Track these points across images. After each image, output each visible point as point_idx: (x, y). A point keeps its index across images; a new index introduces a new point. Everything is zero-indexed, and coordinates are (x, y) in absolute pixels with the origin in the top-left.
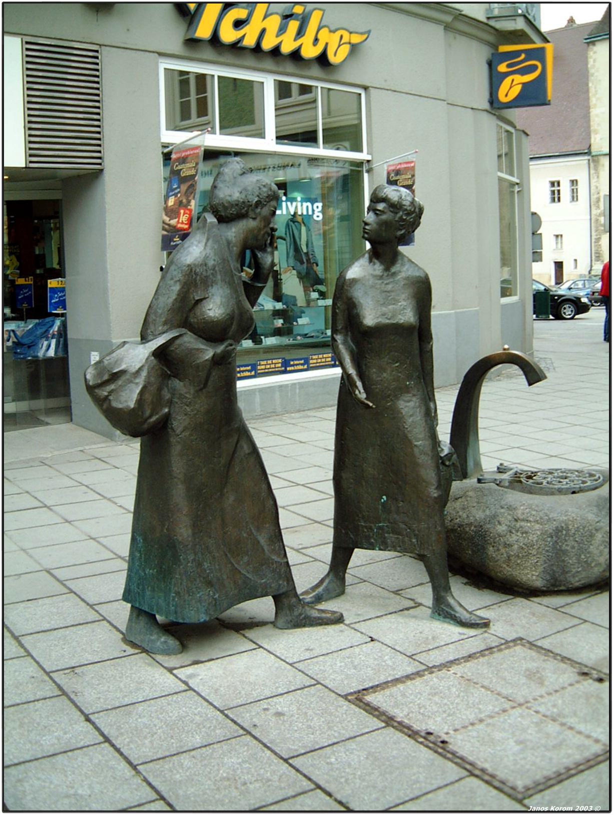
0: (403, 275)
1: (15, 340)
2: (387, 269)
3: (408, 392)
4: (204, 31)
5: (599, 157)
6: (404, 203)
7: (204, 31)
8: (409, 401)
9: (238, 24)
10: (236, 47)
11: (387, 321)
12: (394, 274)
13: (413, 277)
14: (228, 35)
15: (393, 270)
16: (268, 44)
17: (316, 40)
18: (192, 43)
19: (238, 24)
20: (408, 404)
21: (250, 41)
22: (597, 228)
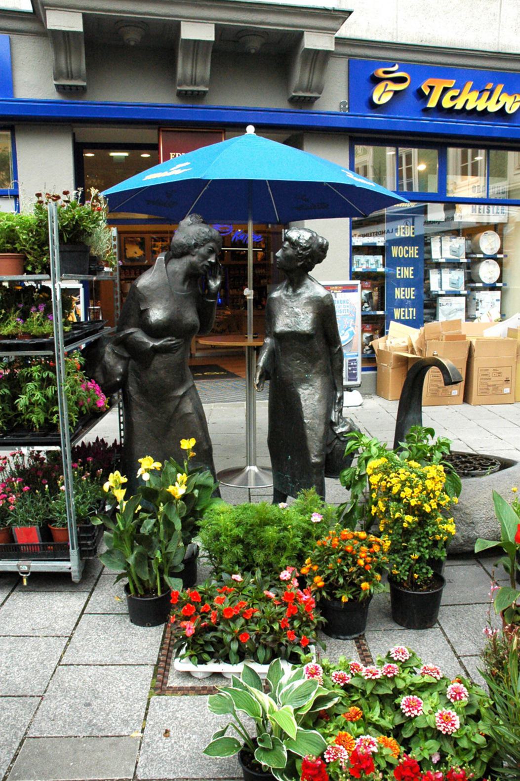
0: (306, 295)
1: (91, 302)
2: (294, 291)
3: (307, 383)
4: (432, 104)
5: (169, 272)
6: (301, 241)
7: (432, 104)
8: (305, 389)
9: (453, 98)
10: (451, 110)
11: (290, 330)
12: (300, 294)
13: (313, 297)
14: (447, 103)
15: (299, 291)
16: (469, 107)
17: (498, 101)
18: (427, 111)
19: (453, 98)
20: (305, 391)
21: (459, 107)
22: (69, 406)
